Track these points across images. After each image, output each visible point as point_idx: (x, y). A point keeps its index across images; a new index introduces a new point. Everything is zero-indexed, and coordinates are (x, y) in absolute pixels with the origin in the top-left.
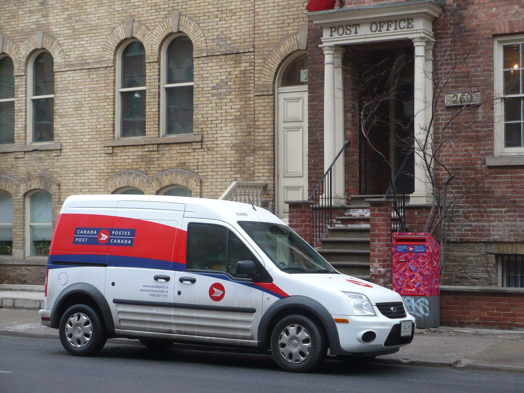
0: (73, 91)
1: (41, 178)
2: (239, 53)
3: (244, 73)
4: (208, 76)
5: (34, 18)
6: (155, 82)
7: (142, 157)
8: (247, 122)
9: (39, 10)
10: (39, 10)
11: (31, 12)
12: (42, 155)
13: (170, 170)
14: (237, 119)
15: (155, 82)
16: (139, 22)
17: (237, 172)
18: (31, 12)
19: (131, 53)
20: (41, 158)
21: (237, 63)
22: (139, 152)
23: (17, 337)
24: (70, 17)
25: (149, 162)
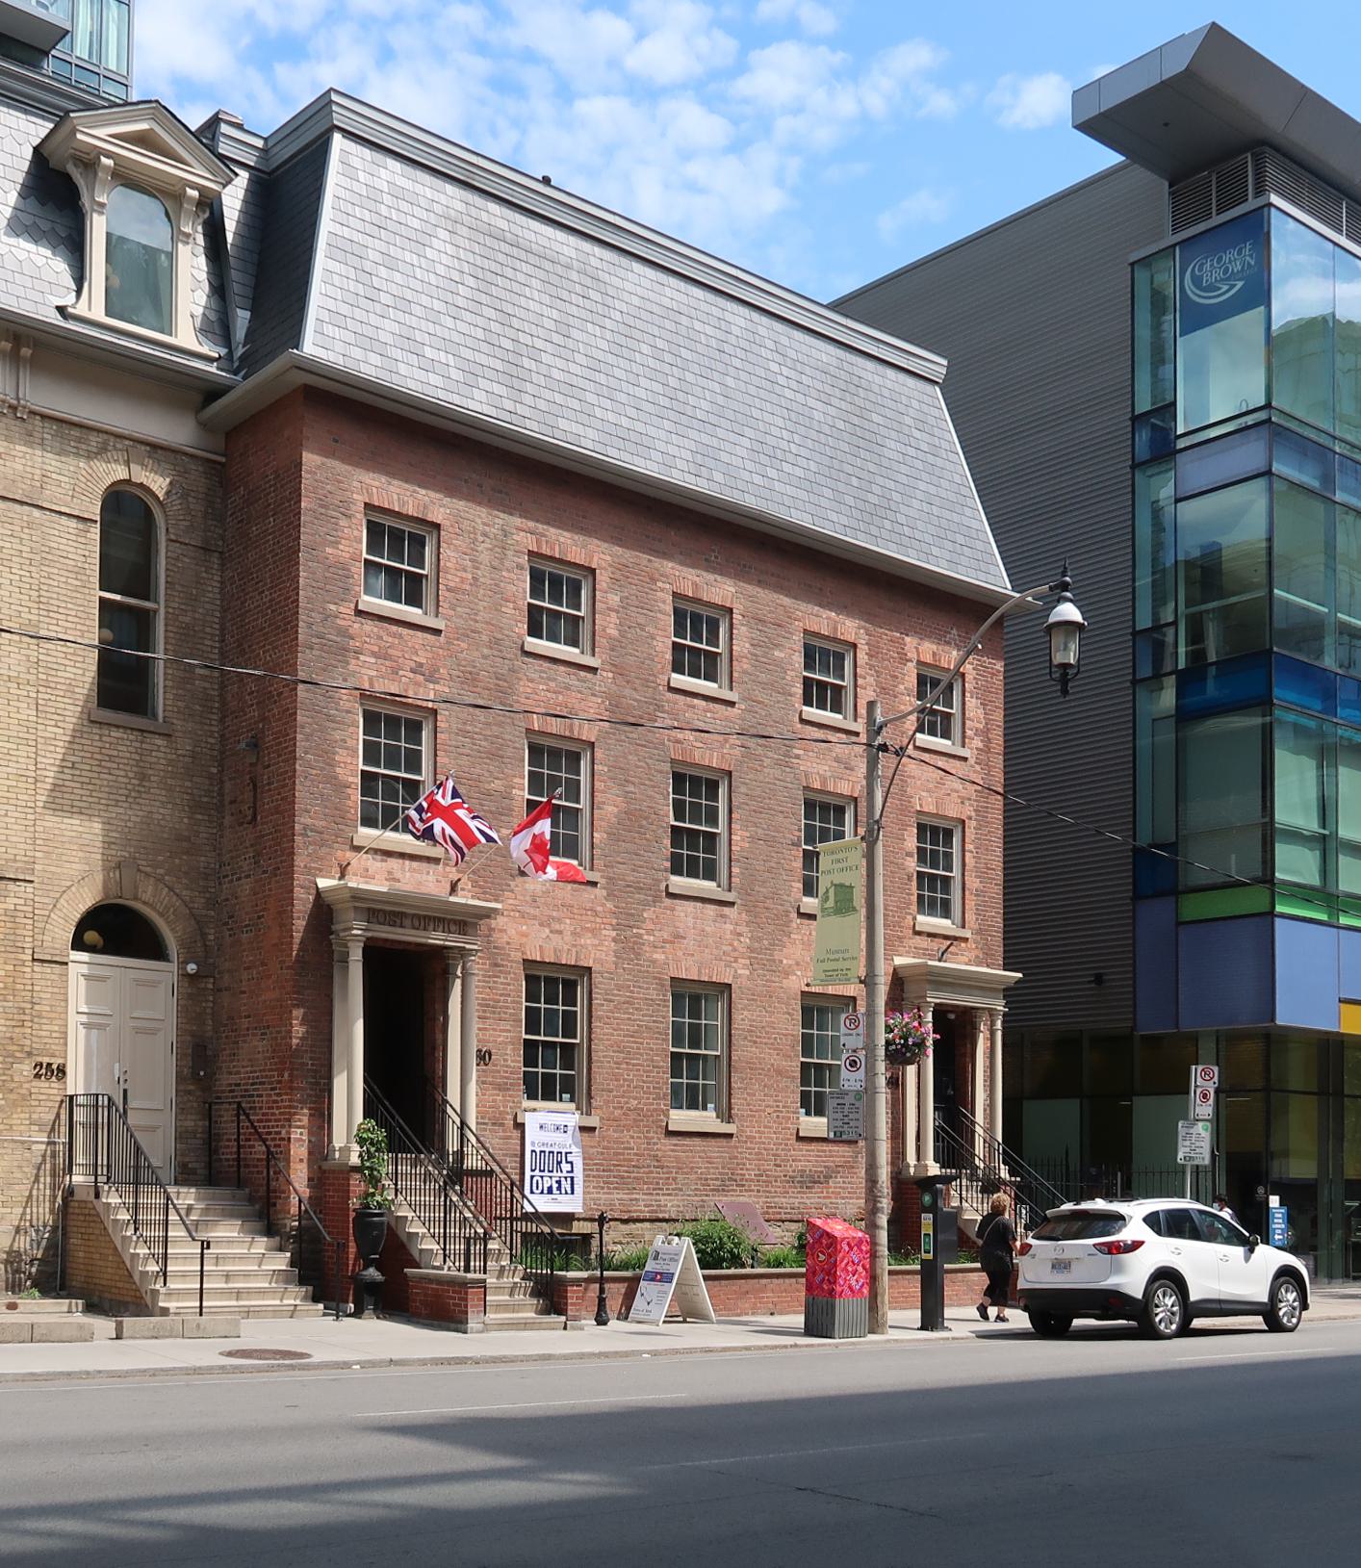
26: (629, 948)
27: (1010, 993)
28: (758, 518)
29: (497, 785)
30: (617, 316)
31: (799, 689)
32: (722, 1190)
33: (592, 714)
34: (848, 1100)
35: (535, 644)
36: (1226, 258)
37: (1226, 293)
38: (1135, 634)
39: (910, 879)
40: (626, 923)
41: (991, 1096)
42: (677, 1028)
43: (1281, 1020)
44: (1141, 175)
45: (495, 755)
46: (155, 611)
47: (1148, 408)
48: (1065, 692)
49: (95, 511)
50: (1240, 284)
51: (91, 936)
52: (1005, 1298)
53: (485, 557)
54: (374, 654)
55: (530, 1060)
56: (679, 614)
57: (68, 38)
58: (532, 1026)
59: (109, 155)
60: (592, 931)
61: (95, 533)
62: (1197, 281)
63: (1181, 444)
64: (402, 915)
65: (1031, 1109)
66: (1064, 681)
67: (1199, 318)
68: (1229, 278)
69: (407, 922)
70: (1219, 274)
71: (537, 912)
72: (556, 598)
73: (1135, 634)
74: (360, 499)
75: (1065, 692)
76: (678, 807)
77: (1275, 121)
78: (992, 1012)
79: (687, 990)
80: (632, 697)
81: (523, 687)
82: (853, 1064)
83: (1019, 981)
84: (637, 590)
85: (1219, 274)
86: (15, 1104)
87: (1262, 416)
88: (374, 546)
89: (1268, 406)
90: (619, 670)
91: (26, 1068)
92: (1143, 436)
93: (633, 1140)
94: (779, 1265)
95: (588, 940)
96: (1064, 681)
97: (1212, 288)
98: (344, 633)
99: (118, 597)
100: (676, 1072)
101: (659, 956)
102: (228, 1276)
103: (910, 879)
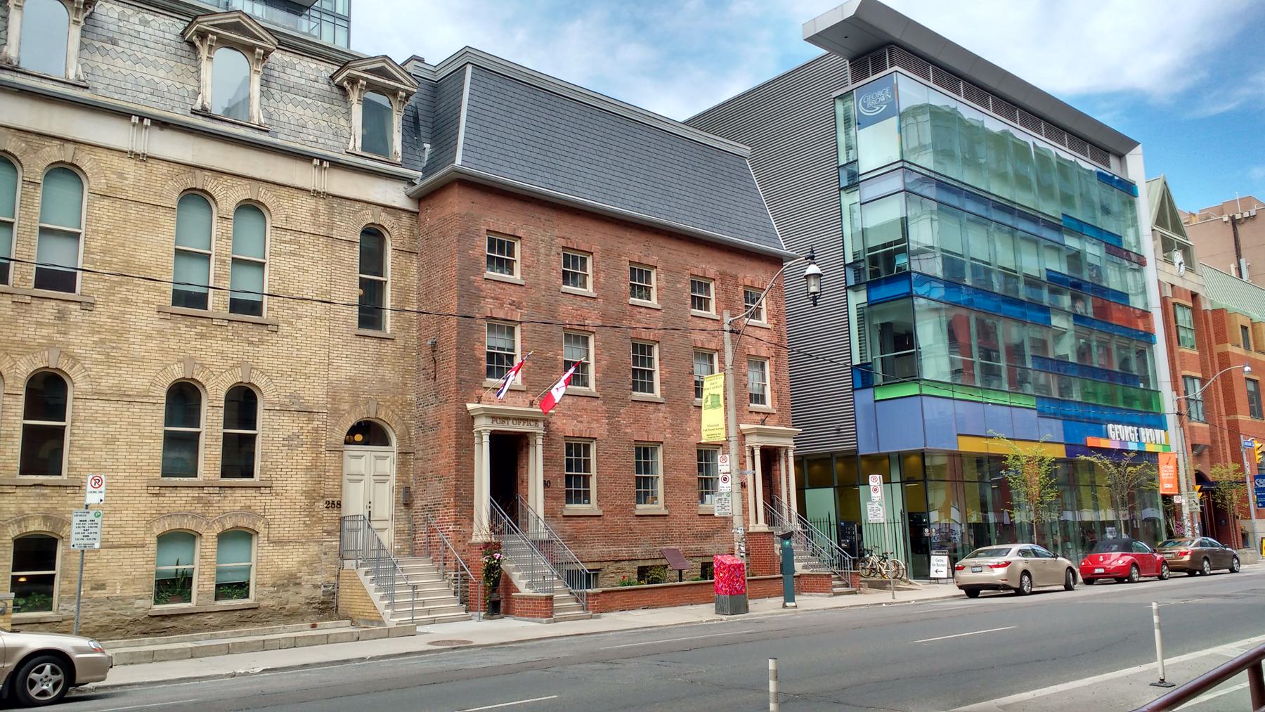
0: (103, 422)
1: (46, 518)
2: (1239, 256)
3: (316, 430)
4: (270, 429)
5: (45, 332)
6: (211, 425)
7: (199, 499)
8: (317, 472)
9: (53, 325)
10: (53, 325)
11: (40, 324)
12: (47, 491)
13: (234, 514)
14: (308, 469)
15: (211, 425)
16: (202, 365)
17: (307, 516)
18: (40, 324)
19: (183, 398)
20: (43, 495)
21: (310, 420)
22: (196, 493)
23: (295, 59)
24: (102, 342)
25: (208, 504)
26: (614, 427)
27: (796, 440)
28: (533, 74)
29: (550, 354)
31: (689, 301)
32: (663, 543)
34: (724, 497)
35: (566, 288)
36: (878, 94)
37: (878, 111)
38: (845, 266)
40: (612, 416)
41: (788, 495)
42: (638, 464)
44: (836, 58)
45: (549, 341)
48: (815, 305)
49: (357, 238)
53: (542, 251)
55: (568, 484)
56: (633, 270)
58: (569, 468)
59: (363, 78)
61: (357, 248)
62: (865, 105)
63: (861, 178)
65: (810, 494)
66: (815, 299)
67: (863, 123)
68: (880, 104)
72: (575, 267)
73: (845, 266)
74: (484, 228)
75: (815, 305)
76: (635, 358)
77: (897, 34)
78: (787, 449)
79: (642, 446)
80: (612, 309)
82: (725, 479)
84: (609, 257)
86: (315, 523)
87: (900, 164)
88: (491, 248)
89: (902, 160)
90: (606, 299)
91: (322, 504)
92: (843, 174)
93: (618, 520)
94: (743, 485)
95: (594, 425)
96: (815, 299)
98: (478, 289)
100: (638, 486)
101: (628, 430)
102: (424, 603)
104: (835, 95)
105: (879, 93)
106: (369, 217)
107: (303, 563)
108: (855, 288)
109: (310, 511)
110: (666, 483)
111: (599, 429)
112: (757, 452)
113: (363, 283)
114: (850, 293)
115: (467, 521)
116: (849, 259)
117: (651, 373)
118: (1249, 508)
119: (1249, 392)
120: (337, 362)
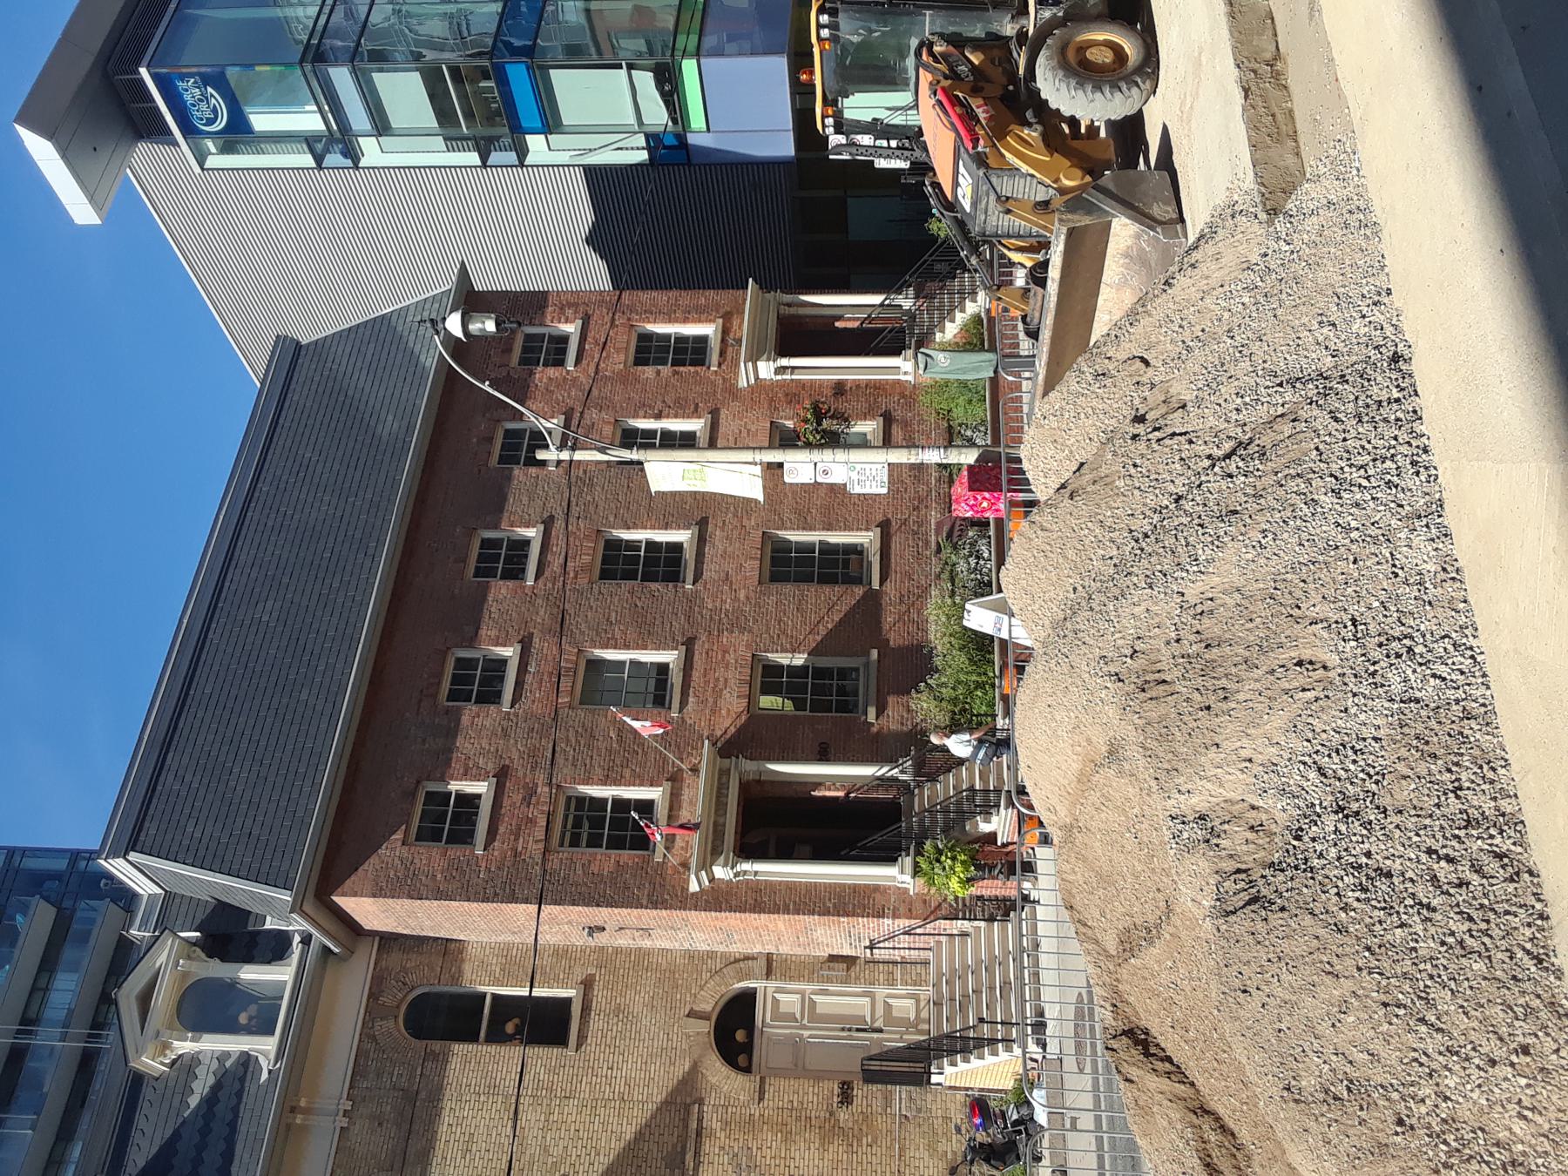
14: (788, 1138)
17: (859, 1140)
26: (737, 623)
30: (308, 455)
33: (555, 651)
34: (854, 476)
37: (217, 100)
39: (676, 373)
43: (654, 488)
46: (495, 997)
47: (310, 156)
50: (210, 90)
51: (742, 1060)
52: (920, 647)
54: (516, 839)
57: (349, 163)
60: (725, 652)
64: (715, 824)
68: (205, 98)
69: (721, 820)
70: (203, 106)
71: (711, 700)
73: (484, 165)
81: (537, 708)
83: (755, 280)
85: (203, 106)
95: (731, 658)
97: (215, 111)
99: (486, 1011)
103: (676, 373)
104: (197, 170)
105: (188, 97)
106: (394, 1028)
107: (931, 1148)
108: (522, 152)
109: (851, 1137)
110: (829, 527)
111: (739, 646)
112: (784, 362)
113: (497, 1036)
114: (529, 160)
115: (877, 896)
116: (473, 158)
117: (651, 545)
118: (632, 662)
119: (25, 914)
120: (619, 1086)
